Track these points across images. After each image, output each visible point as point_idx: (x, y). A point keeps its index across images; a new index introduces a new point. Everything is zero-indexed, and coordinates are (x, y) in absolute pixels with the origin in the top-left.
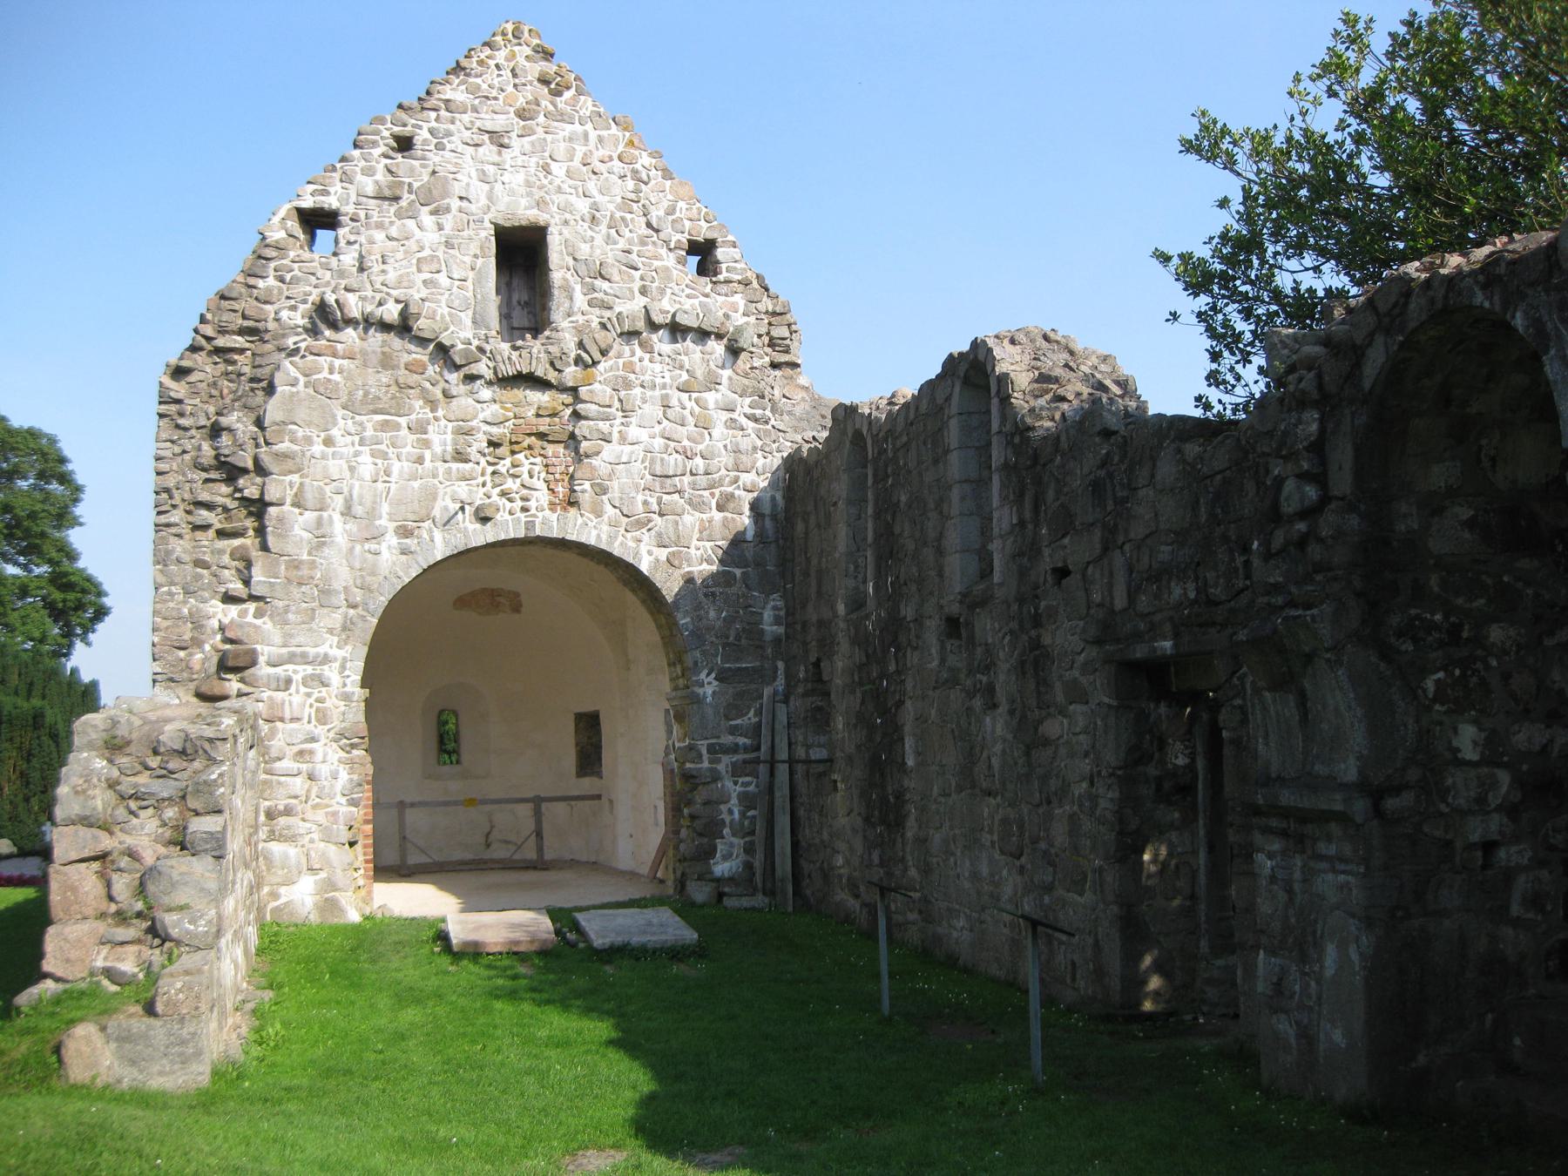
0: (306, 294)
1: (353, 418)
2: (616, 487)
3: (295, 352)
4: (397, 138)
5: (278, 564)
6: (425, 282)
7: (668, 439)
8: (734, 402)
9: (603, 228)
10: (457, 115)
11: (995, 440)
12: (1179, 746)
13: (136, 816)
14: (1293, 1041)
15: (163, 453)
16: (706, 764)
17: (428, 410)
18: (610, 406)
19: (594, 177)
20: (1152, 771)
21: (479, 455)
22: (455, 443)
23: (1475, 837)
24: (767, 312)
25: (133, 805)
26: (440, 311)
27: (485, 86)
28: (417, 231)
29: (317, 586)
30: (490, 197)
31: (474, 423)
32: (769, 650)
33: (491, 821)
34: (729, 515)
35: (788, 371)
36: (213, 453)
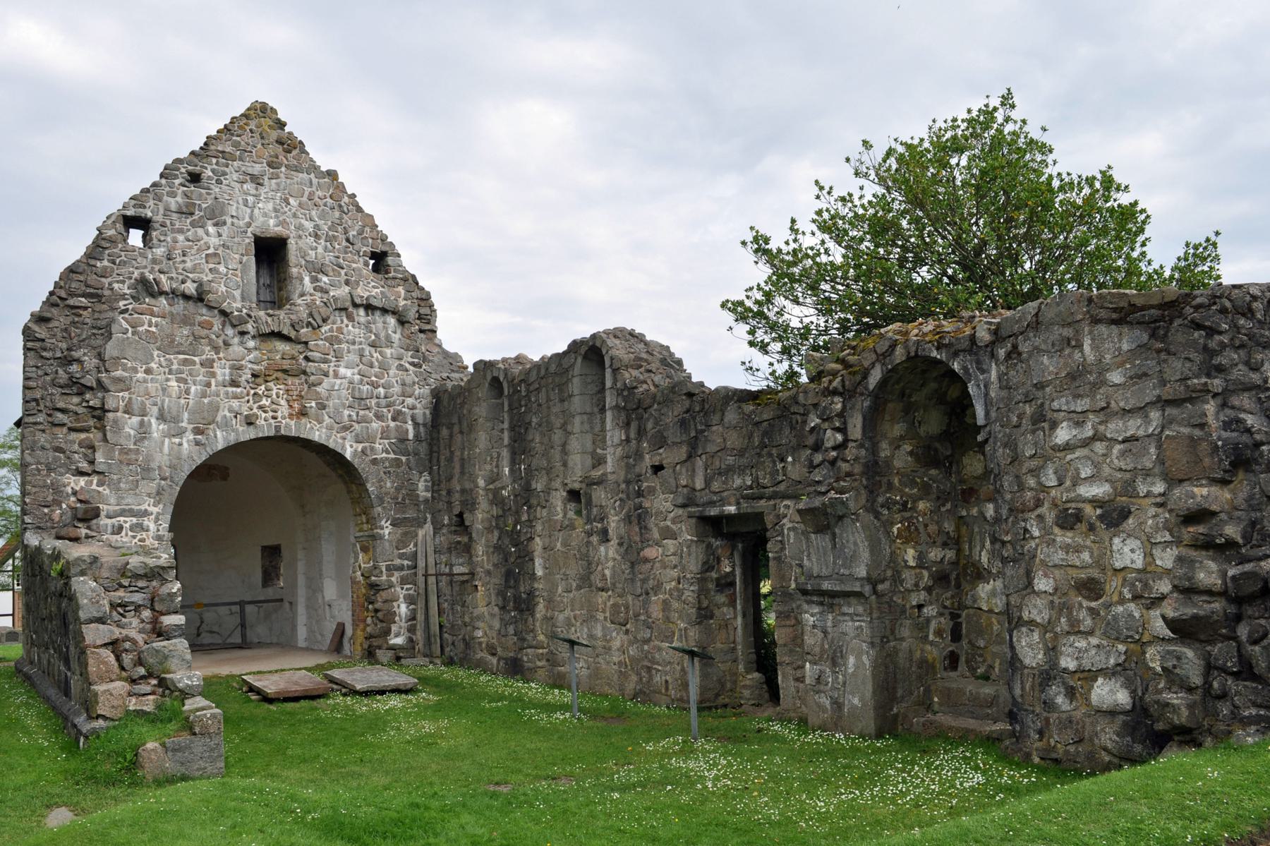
0: (130, 273)
4: (190, 174)
5: (114, 451)
6: (210, 270)
8: (402, 354)
11: (608, 393)
12: (727, 562)
13: (124, 617)
14: (829, 707)
16: (384, 578)
20: (714, 575)
22: (231, 375)
23: (914, 603)
28: (205, 237)
31: (243, 362)
33: (201, 618)
35: (430, 334)
36: (67, 376)
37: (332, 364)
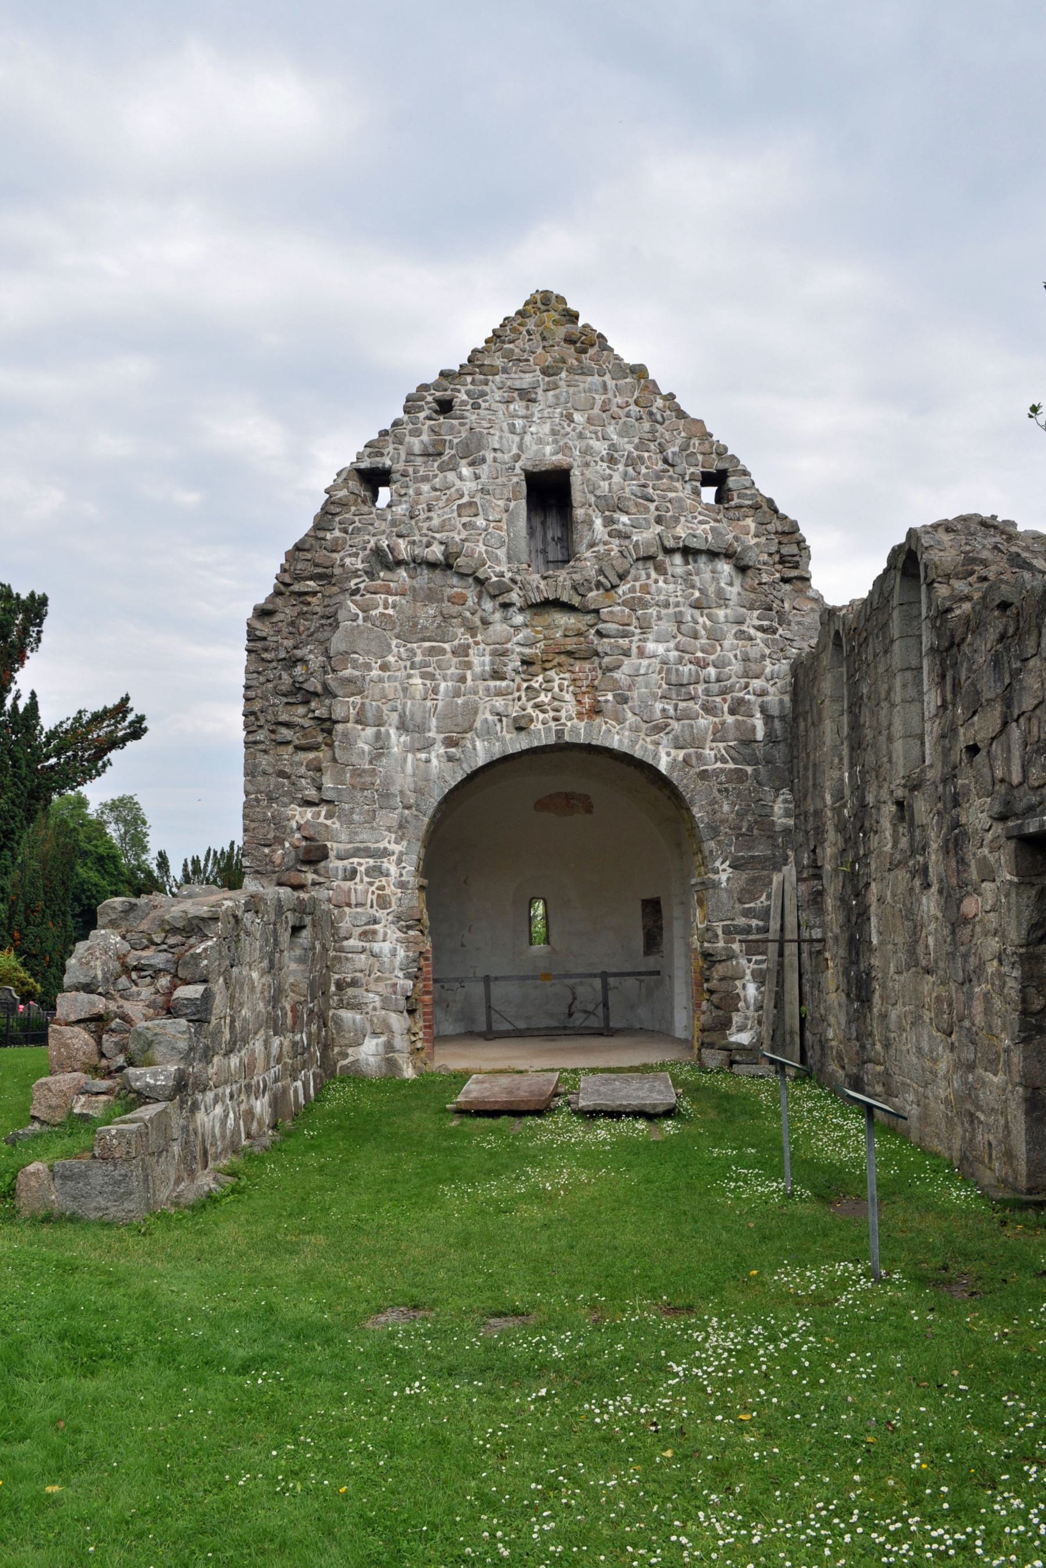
1: (405, 646)
2: (635, 696)
3: (355, 592)
5: (344, 772)
6: (464, 525)
7: (683, 651)
9: (621, 467)
10: (490, 377)
13: (136, 985)
15: (251, 683)
16: (721, 944)
17: (468, 636)
18: (628, 625)
19: (613, 421)
21: (513, 674)
22: (492, 663)
24: (776, 533)
25: (134, 975)
26: (478, 550)
27: (517, 350)
29: (377, 791)
30: (520, 447)
31: (509, 646)
32: (780, 840)
33: (574, 994)
34: (740, 718)
37: (635, 638)
